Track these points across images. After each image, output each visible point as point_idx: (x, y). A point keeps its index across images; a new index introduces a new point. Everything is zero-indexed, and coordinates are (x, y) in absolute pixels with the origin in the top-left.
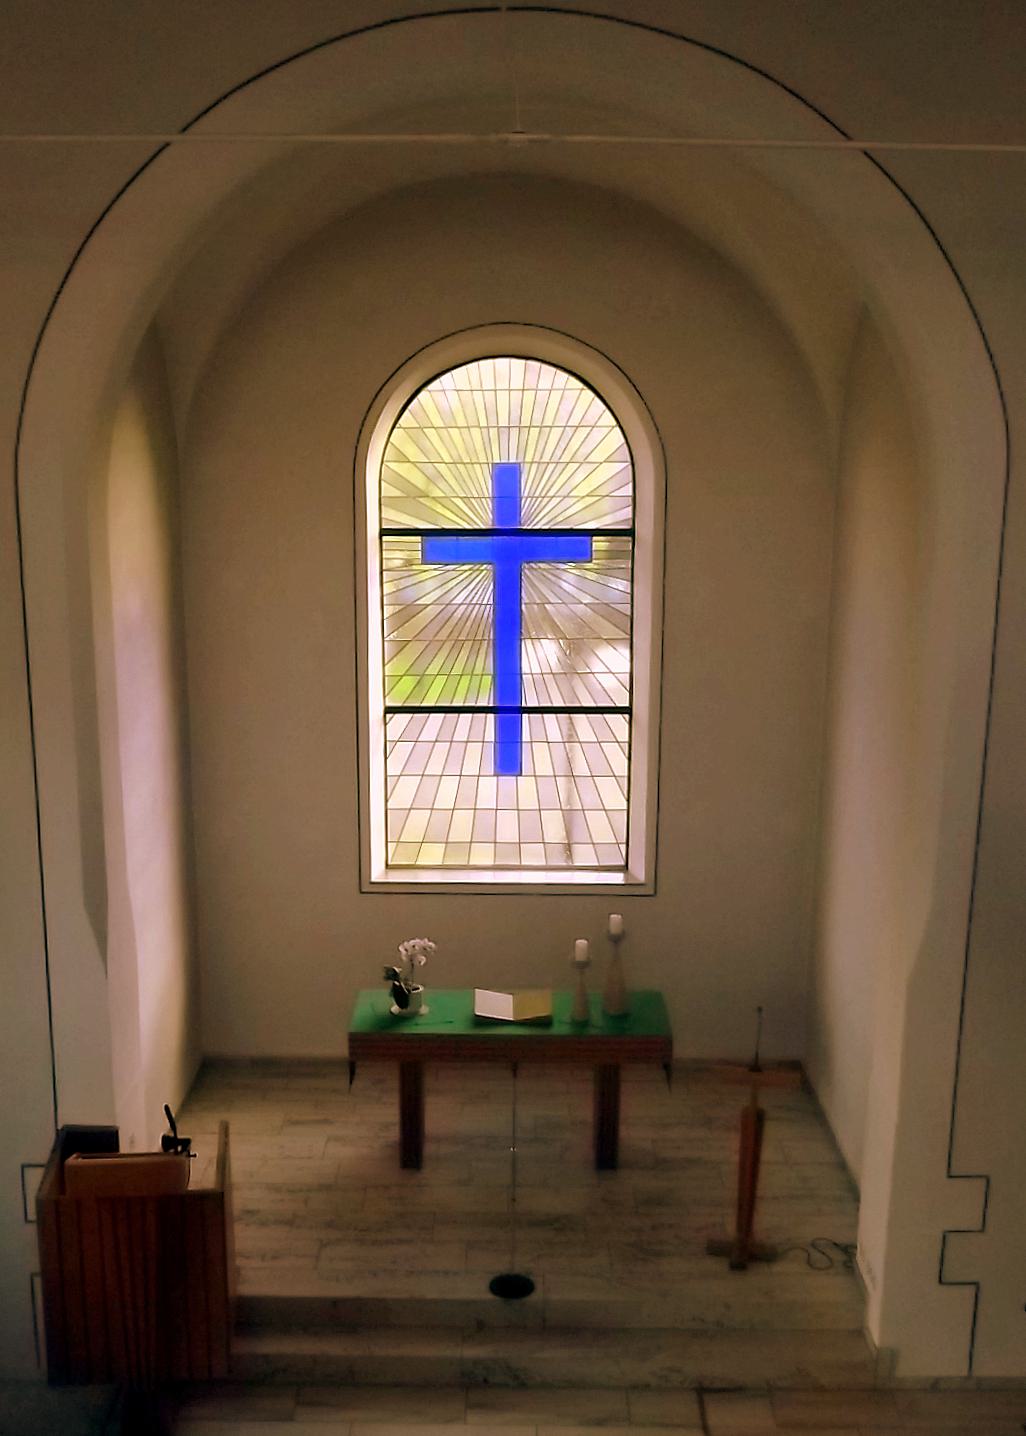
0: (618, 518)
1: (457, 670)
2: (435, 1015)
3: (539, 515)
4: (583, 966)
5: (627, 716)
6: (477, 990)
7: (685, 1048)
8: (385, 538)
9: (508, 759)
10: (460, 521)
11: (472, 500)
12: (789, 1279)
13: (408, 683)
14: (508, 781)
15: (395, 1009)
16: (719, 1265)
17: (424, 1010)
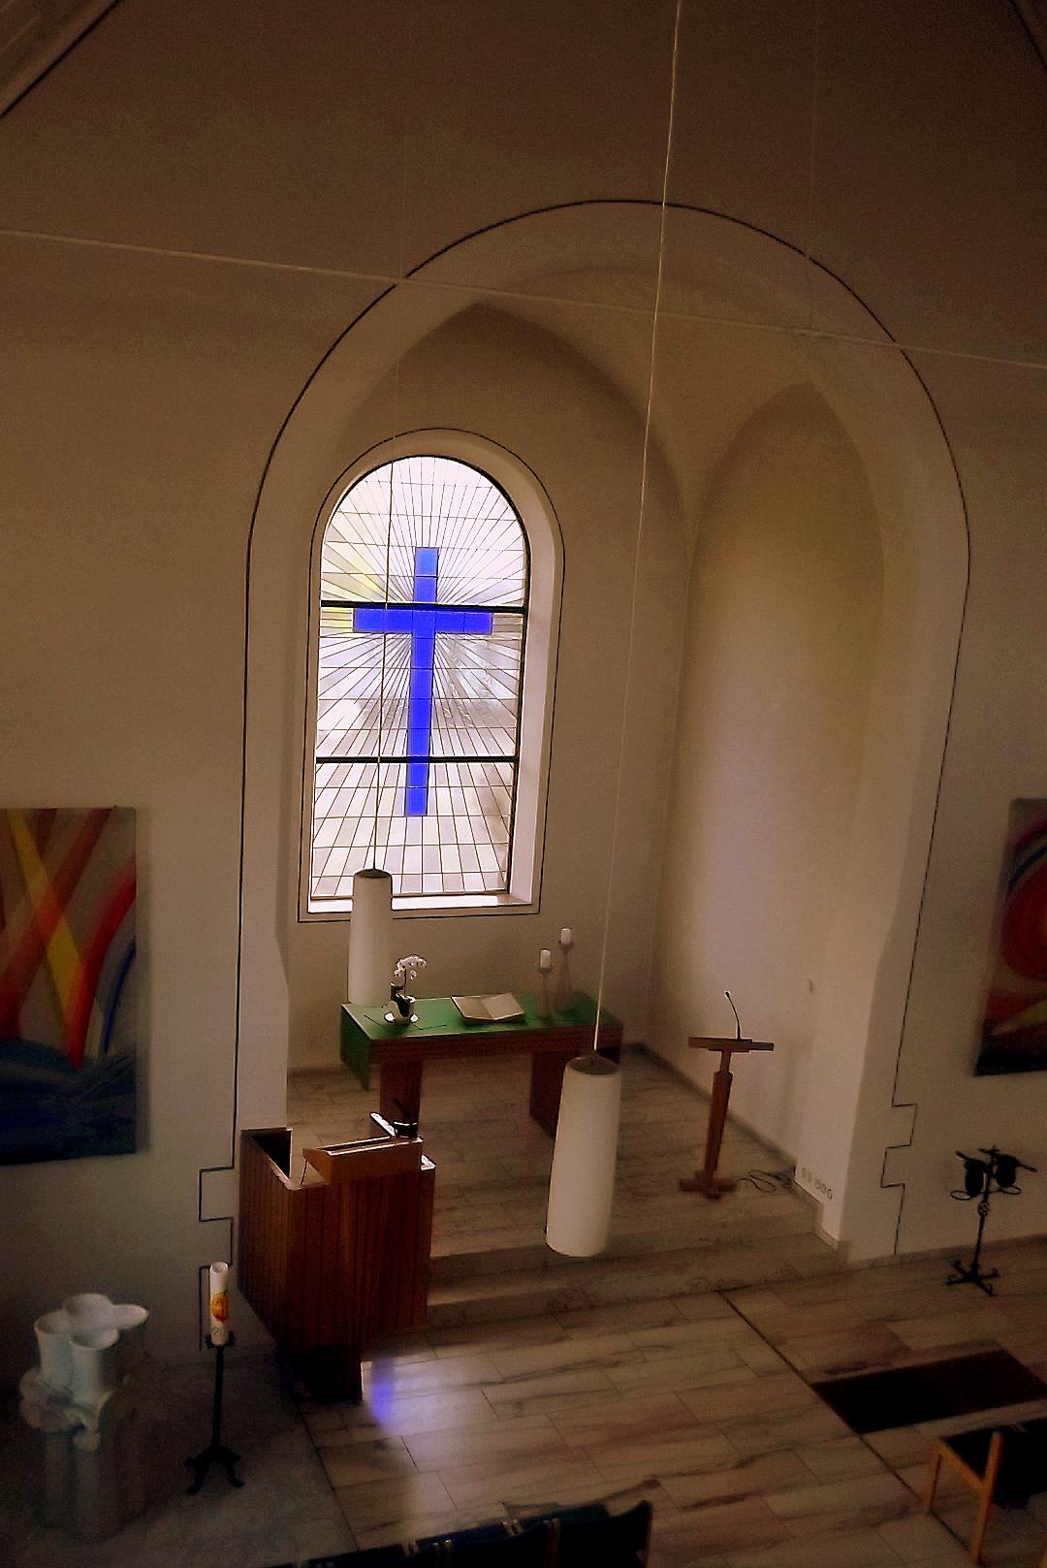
0: (515, 598)
3: (454, 589)
4: (545, 972)
9: (416, 803)
11: (398, 578)
12: (746, 1201)
14: (415, 820)
16: (697, 1198)
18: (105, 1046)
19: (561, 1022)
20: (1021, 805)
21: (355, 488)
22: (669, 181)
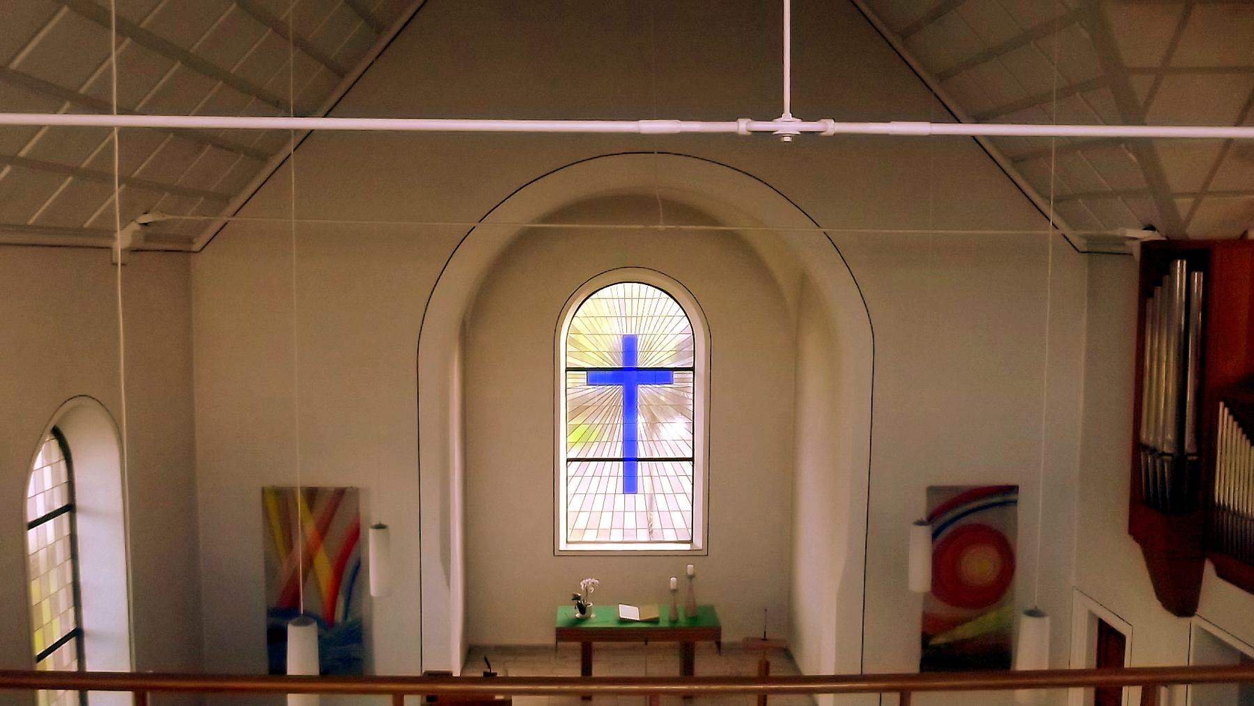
1: (605, 439)
2: (598, 618)
3: (645, 360)
4: (674, 591)
5: (691, 462)
6: (620, 605)
7: (726, 638)
8: (568, 372)
9: (630, 485)
10: (605, 363)
13: (579, 446)
14: (630, 497)
15: (578, 615)
17: (593, 616)
18: (346, 616)
19: (683, 622)
20: (932, 491)
21: (580, 309)
22: (122, 281)
